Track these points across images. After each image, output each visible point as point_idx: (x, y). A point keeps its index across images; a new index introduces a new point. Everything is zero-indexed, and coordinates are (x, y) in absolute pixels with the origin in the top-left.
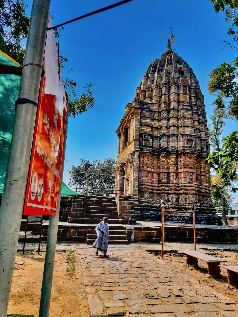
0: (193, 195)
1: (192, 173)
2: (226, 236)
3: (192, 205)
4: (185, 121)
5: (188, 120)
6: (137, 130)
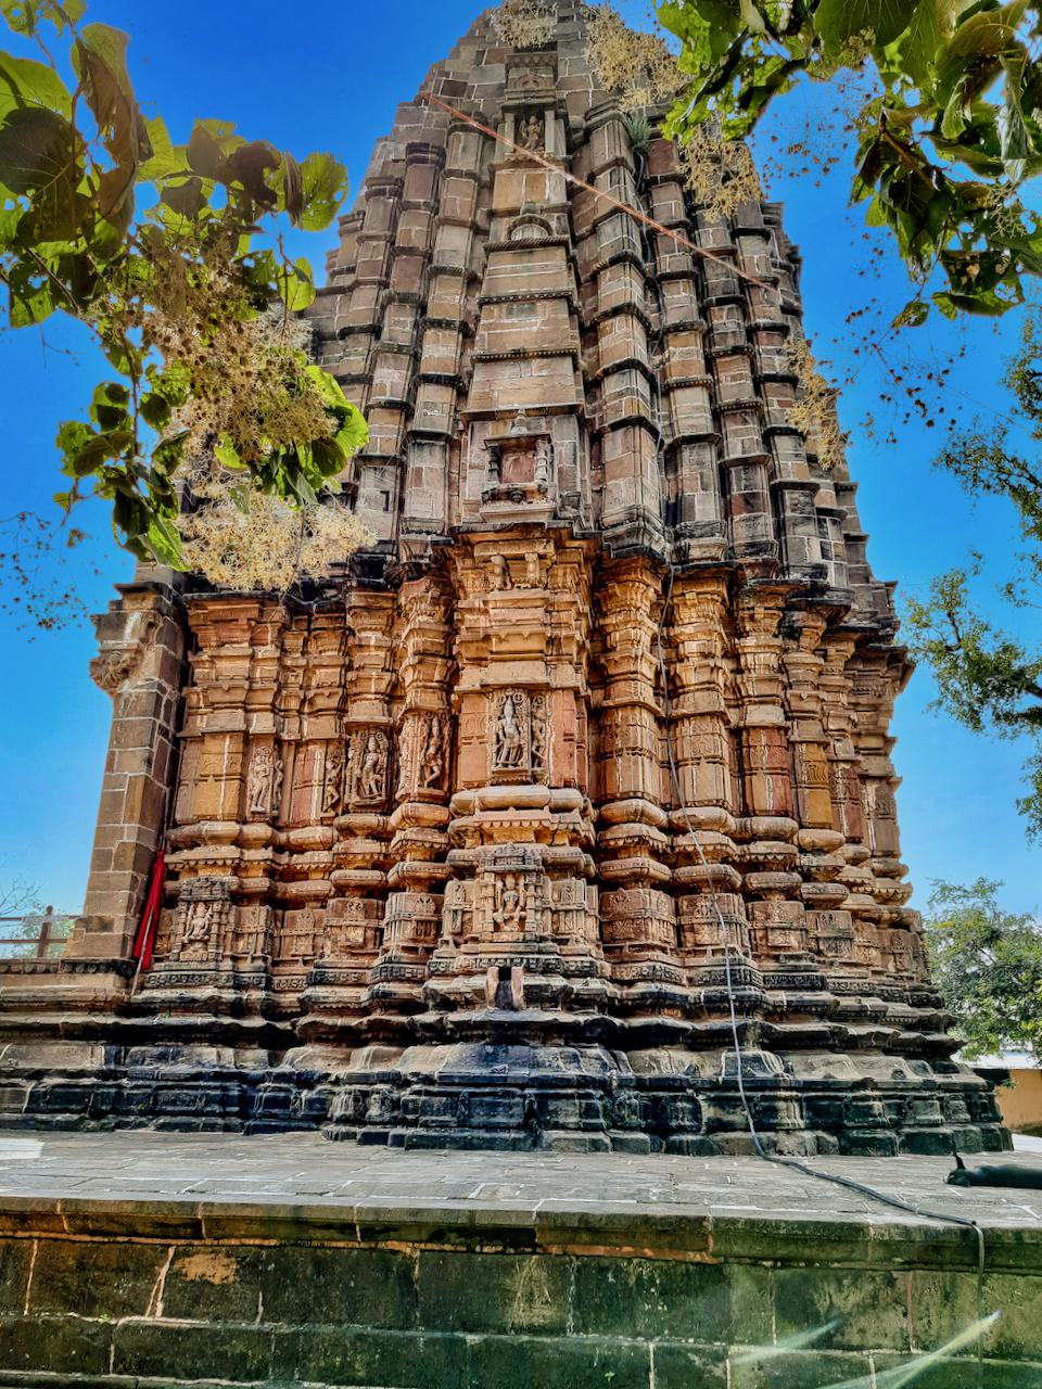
0: (516, 874)
1: (535, 691)
2: (507, 1296)
4: (503, 326)
5: (532, 311)
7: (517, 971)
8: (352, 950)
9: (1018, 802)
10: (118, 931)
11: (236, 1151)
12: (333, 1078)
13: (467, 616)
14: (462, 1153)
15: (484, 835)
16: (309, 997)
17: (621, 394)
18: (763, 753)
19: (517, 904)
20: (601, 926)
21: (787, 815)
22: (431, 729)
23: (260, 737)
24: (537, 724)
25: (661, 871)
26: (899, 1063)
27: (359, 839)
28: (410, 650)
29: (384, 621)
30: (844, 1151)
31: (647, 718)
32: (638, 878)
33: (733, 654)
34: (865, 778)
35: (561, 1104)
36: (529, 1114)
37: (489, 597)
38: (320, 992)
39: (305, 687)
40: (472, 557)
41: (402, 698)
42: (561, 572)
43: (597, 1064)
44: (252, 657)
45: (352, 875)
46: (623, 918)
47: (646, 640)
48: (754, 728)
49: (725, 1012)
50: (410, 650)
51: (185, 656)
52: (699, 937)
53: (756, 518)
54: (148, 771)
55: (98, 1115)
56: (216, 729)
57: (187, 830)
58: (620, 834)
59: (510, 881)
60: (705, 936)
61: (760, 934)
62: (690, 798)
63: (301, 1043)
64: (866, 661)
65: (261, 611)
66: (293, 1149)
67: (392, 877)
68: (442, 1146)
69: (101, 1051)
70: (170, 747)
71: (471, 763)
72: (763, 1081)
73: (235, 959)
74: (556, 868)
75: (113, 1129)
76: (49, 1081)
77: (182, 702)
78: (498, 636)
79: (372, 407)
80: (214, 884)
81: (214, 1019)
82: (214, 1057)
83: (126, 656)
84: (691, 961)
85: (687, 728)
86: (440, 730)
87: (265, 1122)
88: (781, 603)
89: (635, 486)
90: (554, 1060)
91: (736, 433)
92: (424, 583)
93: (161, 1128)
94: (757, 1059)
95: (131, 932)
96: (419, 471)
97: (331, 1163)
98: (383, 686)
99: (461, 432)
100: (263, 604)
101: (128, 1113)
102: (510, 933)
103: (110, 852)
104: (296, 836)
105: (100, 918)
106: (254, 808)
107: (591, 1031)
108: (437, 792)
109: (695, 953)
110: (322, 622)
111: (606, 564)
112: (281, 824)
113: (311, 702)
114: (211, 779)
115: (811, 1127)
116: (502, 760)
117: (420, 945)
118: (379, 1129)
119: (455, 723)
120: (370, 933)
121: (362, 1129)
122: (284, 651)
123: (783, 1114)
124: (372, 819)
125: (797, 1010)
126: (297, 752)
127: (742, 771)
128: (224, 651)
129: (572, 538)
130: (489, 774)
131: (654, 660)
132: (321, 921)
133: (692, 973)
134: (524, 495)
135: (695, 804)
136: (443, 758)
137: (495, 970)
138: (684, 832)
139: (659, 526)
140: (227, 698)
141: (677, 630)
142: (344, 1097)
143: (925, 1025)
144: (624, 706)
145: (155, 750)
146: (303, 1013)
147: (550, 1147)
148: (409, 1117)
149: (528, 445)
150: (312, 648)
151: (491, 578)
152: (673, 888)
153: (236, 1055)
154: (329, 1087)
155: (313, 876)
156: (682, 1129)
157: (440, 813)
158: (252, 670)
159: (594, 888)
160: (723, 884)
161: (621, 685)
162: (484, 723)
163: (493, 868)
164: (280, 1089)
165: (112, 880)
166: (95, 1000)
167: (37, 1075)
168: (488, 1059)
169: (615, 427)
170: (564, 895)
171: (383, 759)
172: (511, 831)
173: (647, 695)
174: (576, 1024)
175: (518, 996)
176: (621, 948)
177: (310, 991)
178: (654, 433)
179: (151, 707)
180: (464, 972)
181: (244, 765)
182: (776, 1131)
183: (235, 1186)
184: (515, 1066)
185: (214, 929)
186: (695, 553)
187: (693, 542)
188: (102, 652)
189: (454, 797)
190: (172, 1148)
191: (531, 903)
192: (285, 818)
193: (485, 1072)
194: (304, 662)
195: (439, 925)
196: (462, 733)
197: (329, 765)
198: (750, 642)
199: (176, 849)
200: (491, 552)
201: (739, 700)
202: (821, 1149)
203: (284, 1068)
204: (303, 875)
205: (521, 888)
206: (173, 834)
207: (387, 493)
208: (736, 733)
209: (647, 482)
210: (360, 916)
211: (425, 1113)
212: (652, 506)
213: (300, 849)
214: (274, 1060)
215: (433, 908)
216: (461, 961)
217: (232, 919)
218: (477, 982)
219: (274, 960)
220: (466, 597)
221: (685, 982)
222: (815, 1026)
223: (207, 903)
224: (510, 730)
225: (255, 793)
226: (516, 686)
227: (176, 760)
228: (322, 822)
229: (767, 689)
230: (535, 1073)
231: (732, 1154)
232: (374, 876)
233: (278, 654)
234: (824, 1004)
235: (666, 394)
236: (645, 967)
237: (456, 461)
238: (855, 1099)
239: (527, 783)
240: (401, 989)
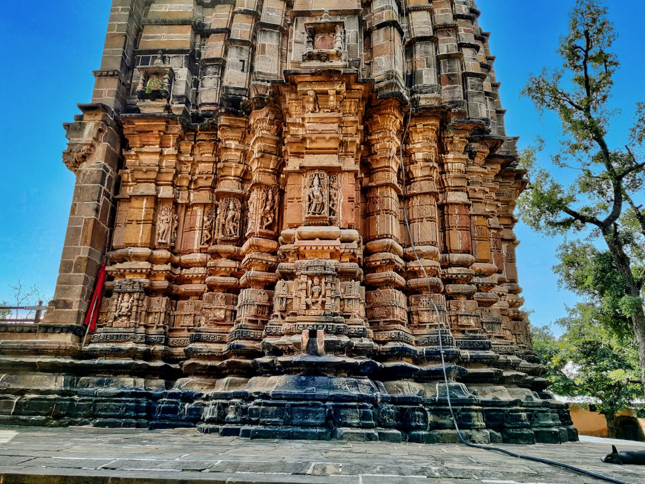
0: (321, 276)
1: (332, 171)
3: (306, 332)
6: (113, 36)
7: (320, 332)
8: (218, 322)
9: (553, 268)
10: (75, 309)
11: (142, 440)
12: (204, 396)
13: (292, 128)
14: (287, 441)
15: (299, 254)
16: (191, 349)
17: (383, 9)
18: (455, 218)
19: (320, 294)
20: (366, 309)
21: (469, 253)
22: (267, 196)
23: (165, 200)
24: (333, 191)
25: (400, 280)
26: (528, 392)
27: (223, 259)
28: (256, 151)
29: (240, 135)
30: (505, 441)
31: (394, 194)
32: (389, 283)
33: (441, 164)
34: (503, 240)
35: (348, 411)
36: (328, 417)
37: (306, 115)
38: (198, 346)
39: (192, 174)
40: (296, 92)
41: (250, 180)
42: (348, 104)
43: (368, 388)
44: (161, 153)
45: (218, 279)
46: (378, 305)
47: (394, 150)
48: (452, 204)
49: (440, 360)
50: (256, 151)
51: (121, 152)
52: (421, 318)
53: (455, 88)
54: (97, 216)
55: (57, 417)
56: (138, 193)
57: (119, 252)
58: (378, 258)
59: (316, 280)
60: (425, 318)
61: (453, 318)
62: (416, 241)
63: (186, 376)
64: (504, 177)
65: (167, 127)
66: (179, 438)
67: (242, 280)
68: (274, 437)
69: (62, 379)
70: (110, 205)
71: (291, 214)
72: (462, 400)
73: (146, 327)
74: (344, 275)
75: (67, 426)
76: (29, 396)
77: (119, 178)
78: (310, 139)
79: (236, 13)
80: (135, 283)
81: (132, 361)
82: (132, 383)
83: (85, 148)
84: (417, 332)
85: (416, 201)
86: (273, 197)
87: (162, 422)
88: (468, 135)
89: (389, 62)
90: (343, 385)
91: (444, 41)
92: (265, 111)
93: (96, 425)
94: (458, 388)
95: (83, 310)
96: (263, 46)
97: (205, 448)
98: (239, 172)
99: (289, 25)
100: (167, 122)
101: (77, 416)
102: (316, 310)
103: (72, 262)
104: (185, 258)
105: (64, 301)
106: (160, 241)
107: (363, 369)
108: (270, 232)
109: (419, 327)
110: (202, 136)
111: (374, 103)
112: (176, 251)
113: (195, 182)
114: (134, 223)
115: (487, 427)
116: (312, 210)
117: (259, 319)
118: (234, 426)
119: (282, 193)
120: (228, 313)
121: (222, 426)
122: (180, 152)
123: (475, 419)
124: (231, 248)
125: (476, 361)
126: (186, 211)
127: (444, 228)
128: (144, 149)
129: (357, 82)
130: (304, 220)
131: (399, 161)
132: (198, 306)
133: (418, 339)
134: (328, 57)
135: (419, 244)
136: (274, 213)
138: (413, 259)
139: (404, 85)
140: (145, 176)
141: (411, 146)
142: (212, 407)
143: (534, 372)
144: (382, 186)
145: (101, 204)
146: (188, 358)
147: (342, 438)
148: (253, 419)
149: (330, 29)
150: (196, 151)
151: (307, 105)
152: (408, 291)
153: (145, 383)
154: (202, 401)
155: (195, 282)
156: (419, 428)
157: (272, 244)
158: (161, 161)
159: (364, 288)
160: (435, 288)
161: (380, 174)
162: (301, 191)
163: (306, 272)
164: (172, 402)
165: (72, 279)
166: (59, 348)
167: (22, 392)
168: (302, 384)
169: (379, 27)
170: (348, 290)
171: (238, 214)
172: (316, 252)
173: (394, 179)
174: (356, 364)
175: (320, 347)
176: (378, 323)
177: (191, 346)
178: (401, 33)
179: (99, 179)
180: (290, 334)
181: (155, 216)
182: (471, 429)
183: (139, 464)
184: (318, 388)
185: (134, 309)
186: (423, 103)
187: (422, 96)
188: (69, 144)
189: (282, 232)
190: (101, 438)
191: (328, 293)
192: (178, 248)
193: (301, 392)
194: (191, 159)
195: (271, 308)
196: (288, 196)
197: (206, 219)
198: (450, 156)
199: (113, 263)
200: (307, 88)
201: (443, 189)
202: (493, 439)
203: (175, 390)
204: (189, 281)
205: (323, 284)
206: (111, 254)
207: (243, 61)
208: (441, 207)
209: (397, 59)
210: (223, 303)
211: (263, 417)
212: (399, 71)
213: (188, 266)
214: (169, 385)
215: (267, 298)
216: (286, 326)
217: (145, 304)
218: (296, 338)
219: (170, 329)
220: (290, 116)
221: (414, 343)
222: (485, 370)
223: (131, 294)
224: (317, 193)
225: (161, 232)
226: (321, 168)
227: (114, 212)
228: (200, 251)
229: (459, 183)
230: (332, 393)
231: (444, 442)
232: (232, 280)
233: (176, 152)
234: (491, 357)
235: (407, 15)
236: (393, 333)
237: (285, 43)
238: (512, 411)
239: (327, 225)
240: (248, 344)
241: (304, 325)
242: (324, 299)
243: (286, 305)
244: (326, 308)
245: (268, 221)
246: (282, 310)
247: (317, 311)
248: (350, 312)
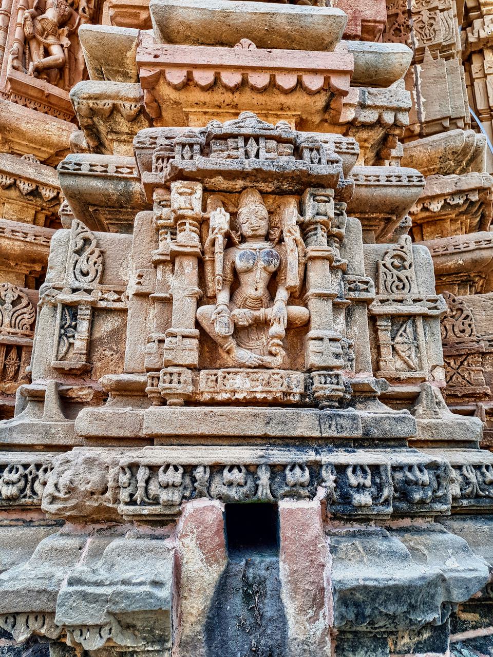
7: (300, 515)
19: (274, 281)
59: (253, 211)
137: (208, 511)
163: (201, 162)
191: (321, 279)
205: (292, 234)
241: (189, 469)
242: (298, 311)
243: (91, 345)
244: (313, 359)
245: (47, 53)
246: (66, 365)
247: (264, 375)
248: (409, 381)
